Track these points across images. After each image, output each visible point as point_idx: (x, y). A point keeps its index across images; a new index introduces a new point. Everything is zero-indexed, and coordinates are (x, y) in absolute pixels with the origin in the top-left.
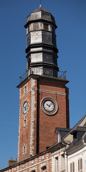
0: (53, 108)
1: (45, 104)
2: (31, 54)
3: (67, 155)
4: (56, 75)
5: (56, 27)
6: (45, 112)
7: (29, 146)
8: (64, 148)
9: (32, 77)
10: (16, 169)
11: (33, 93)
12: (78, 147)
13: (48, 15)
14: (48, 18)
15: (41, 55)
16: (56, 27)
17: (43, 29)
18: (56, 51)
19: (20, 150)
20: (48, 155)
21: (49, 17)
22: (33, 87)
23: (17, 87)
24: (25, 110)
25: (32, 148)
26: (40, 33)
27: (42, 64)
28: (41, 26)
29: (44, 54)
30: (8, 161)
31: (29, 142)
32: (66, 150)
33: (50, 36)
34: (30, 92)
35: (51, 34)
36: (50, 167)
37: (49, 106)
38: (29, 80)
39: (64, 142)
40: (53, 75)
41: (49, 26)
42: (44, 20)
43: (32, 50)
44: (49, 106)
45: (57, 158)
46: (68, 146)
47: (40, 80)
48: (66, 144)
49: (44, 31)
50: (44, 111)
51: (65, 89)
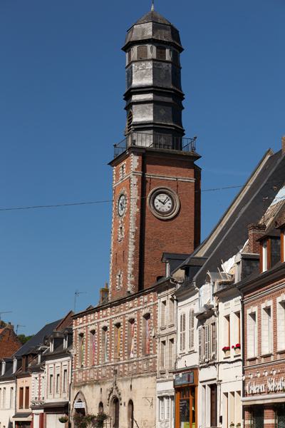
0: (170, 206)
1: (156, 200)
2: (134, 106)
3: (177, 301)
4: (178, 145)
5: (181, 50)
6: (155, 214)
7: (126, 275)
8: (174, 289)
9: (133, 152)
10: (107, 313)
11: (134, 180)
12: (190, 291)
13: (166, 29)
14: (165, 36)
15: (150, 108)
16: (181, 50)
17: (155, 57)
18: (179, 96)
19: (113, 280)
20: (109, 311)
21: (167, 32)
22: (134, 170)
23: (109, 164)
24: (122, 210)
25: (131, 279)
26: (150, 65)
27: (152, 126)
28: (151, 51)
29: (157, 106)
30: (99, 290)
31: (126, 268)
32: (176, 293)
33: (168, 71)
34: (130, 178)
35: (170, 65)
36: (156, 317)
37: (162, 204)
38: (128, 156)
39: (173, 280)
40: (171, 144)
41: (167, 51)
42: (158, 40)
43: (135, 98)
44: (164, 203)
45: (164, 303)
46: (179, 286)
47: (147, 157)
48: (176, 282)
49: (157, 61)
50: (153, 212)
51: (193, 170)
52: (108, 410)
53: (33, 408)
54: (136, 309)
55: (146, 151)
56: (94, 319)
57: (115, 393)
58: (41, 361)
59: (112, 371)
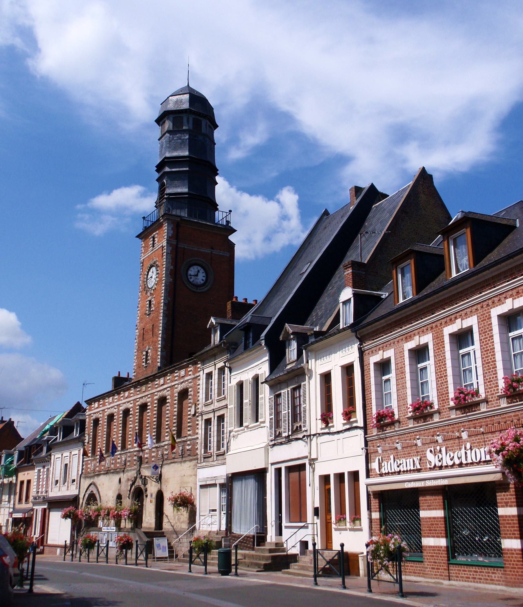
0: (204, 278)
23: (137, 237)
52: (127, 502)
53: (34, 504)
54: (169, 385)
55: (182, 220)
56: (113, 402)
57: (139, 482)
58: (47, 452)
59: (135, 458)
